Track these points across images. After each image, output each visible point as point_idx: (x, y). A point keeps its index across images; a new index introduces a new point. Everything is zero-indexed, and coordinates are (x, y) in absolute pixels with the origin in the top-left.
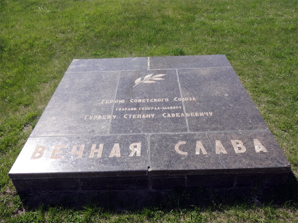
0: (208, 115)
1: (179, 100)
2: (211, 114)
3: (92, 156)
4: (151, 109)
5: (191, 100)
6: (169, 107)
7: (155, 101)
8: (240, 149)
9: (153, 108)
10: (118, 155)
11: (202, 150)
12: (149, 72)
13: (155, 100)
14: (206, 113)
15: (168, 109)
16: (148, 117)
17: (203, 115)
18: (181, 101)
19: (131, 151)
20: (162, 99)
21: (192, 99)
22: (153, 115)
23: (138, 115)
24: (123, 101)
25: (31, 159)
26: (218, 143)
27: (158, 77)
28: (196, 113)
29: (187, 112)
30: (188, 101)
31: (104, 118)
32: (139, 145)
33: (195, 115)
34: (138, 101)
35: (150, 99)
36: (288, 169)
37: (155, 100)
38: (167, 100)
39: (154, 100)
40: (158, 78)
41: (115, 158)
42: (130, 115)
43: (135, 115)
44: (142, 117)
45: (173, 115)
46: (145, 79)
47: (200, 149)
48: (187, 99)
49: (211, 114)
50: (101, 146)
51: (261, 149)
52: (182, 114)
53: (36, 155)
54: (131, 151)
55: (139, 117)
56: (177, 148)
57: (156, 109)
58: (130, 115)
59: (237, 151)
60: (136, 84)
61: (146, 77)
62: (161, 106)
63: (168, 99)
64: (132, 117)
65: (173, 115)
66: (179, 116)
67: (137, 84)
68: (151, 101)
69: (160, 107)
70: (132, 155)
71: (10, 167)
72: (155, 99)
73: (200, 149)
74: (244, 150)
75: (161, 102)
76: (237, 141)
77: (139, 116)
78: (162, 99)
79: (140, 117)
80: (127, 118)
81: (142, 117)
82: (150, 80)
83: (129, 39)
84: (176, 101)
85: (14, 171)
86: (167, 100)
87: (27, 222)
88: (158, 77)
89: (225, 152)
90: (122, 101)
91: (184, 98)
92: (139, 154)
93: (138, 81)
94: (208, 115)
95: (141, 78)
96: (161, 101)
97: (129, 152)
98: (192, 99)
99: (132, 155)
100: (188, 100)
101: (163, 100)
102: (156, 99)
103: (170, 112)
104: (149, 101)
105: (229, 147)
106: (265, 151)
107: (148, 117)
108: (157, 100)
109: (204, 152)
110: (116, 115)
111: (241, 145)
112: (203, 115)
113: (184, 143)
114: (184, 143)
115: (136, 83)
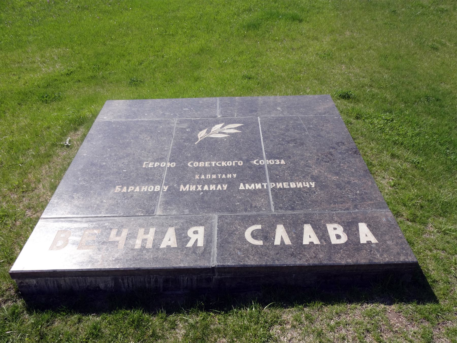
0: (308, 186)
1: (262, 164)
5: (279, 163)
6: (226, 175)
7: (223, 165)
8: (338, 237)
12: (217, 123)
13: (207, 164)
14: (306, 184)
17: (302, 187)
18: (264, 165)
19: (190, 238)
20: (234, 162)
21: (280, 162)
24: (173, 165)
25: (51, 248)
27: (231, 129)
28: (291, 183)
29: (272, 180)
30: (275, 164)
32: (201, 230)
33: (290, 187)
34: (199, 165)
37: (207, 164)
39: (220, 164)
43: (286, 183)
45: (213, 187)
46: (212, 131)
48: (272, 162)
49: (235, 176)
51: (311, 240)
53: (188, 244)
54: (190, 238)
57: (203, 177)
59: (334, 241)
60: (199, 140)
61: (213, 128)
62: (217, 174)
63: (242, 162)
65: (213, 187)
67: (201, 139)
68: (217, 164)
70: (190, 244)
71: (11, 261)
73: (282, 237)
74: (344, 239)
75: (204, 168)
76: (336, 225)
77: (208, 176)
78: (234, 162)
79: (209, 178)
82: (219, 133)
84: (256, 164)
87: (13, 341)
88: (231, 129)
92: (201, 244)
93: (202, 134)
97: (188, 239)
98: (280, 162)
99: (190, 244)
100: (273, 163)
101: (236, 163)
103: (209, 182)
104: (215, 164)
108: (226, 163)
109: (288, 242)
111: (340, 230)
112: (302, 187)
113: (259, 227)
114: (259, 227)
115: (199, 137)
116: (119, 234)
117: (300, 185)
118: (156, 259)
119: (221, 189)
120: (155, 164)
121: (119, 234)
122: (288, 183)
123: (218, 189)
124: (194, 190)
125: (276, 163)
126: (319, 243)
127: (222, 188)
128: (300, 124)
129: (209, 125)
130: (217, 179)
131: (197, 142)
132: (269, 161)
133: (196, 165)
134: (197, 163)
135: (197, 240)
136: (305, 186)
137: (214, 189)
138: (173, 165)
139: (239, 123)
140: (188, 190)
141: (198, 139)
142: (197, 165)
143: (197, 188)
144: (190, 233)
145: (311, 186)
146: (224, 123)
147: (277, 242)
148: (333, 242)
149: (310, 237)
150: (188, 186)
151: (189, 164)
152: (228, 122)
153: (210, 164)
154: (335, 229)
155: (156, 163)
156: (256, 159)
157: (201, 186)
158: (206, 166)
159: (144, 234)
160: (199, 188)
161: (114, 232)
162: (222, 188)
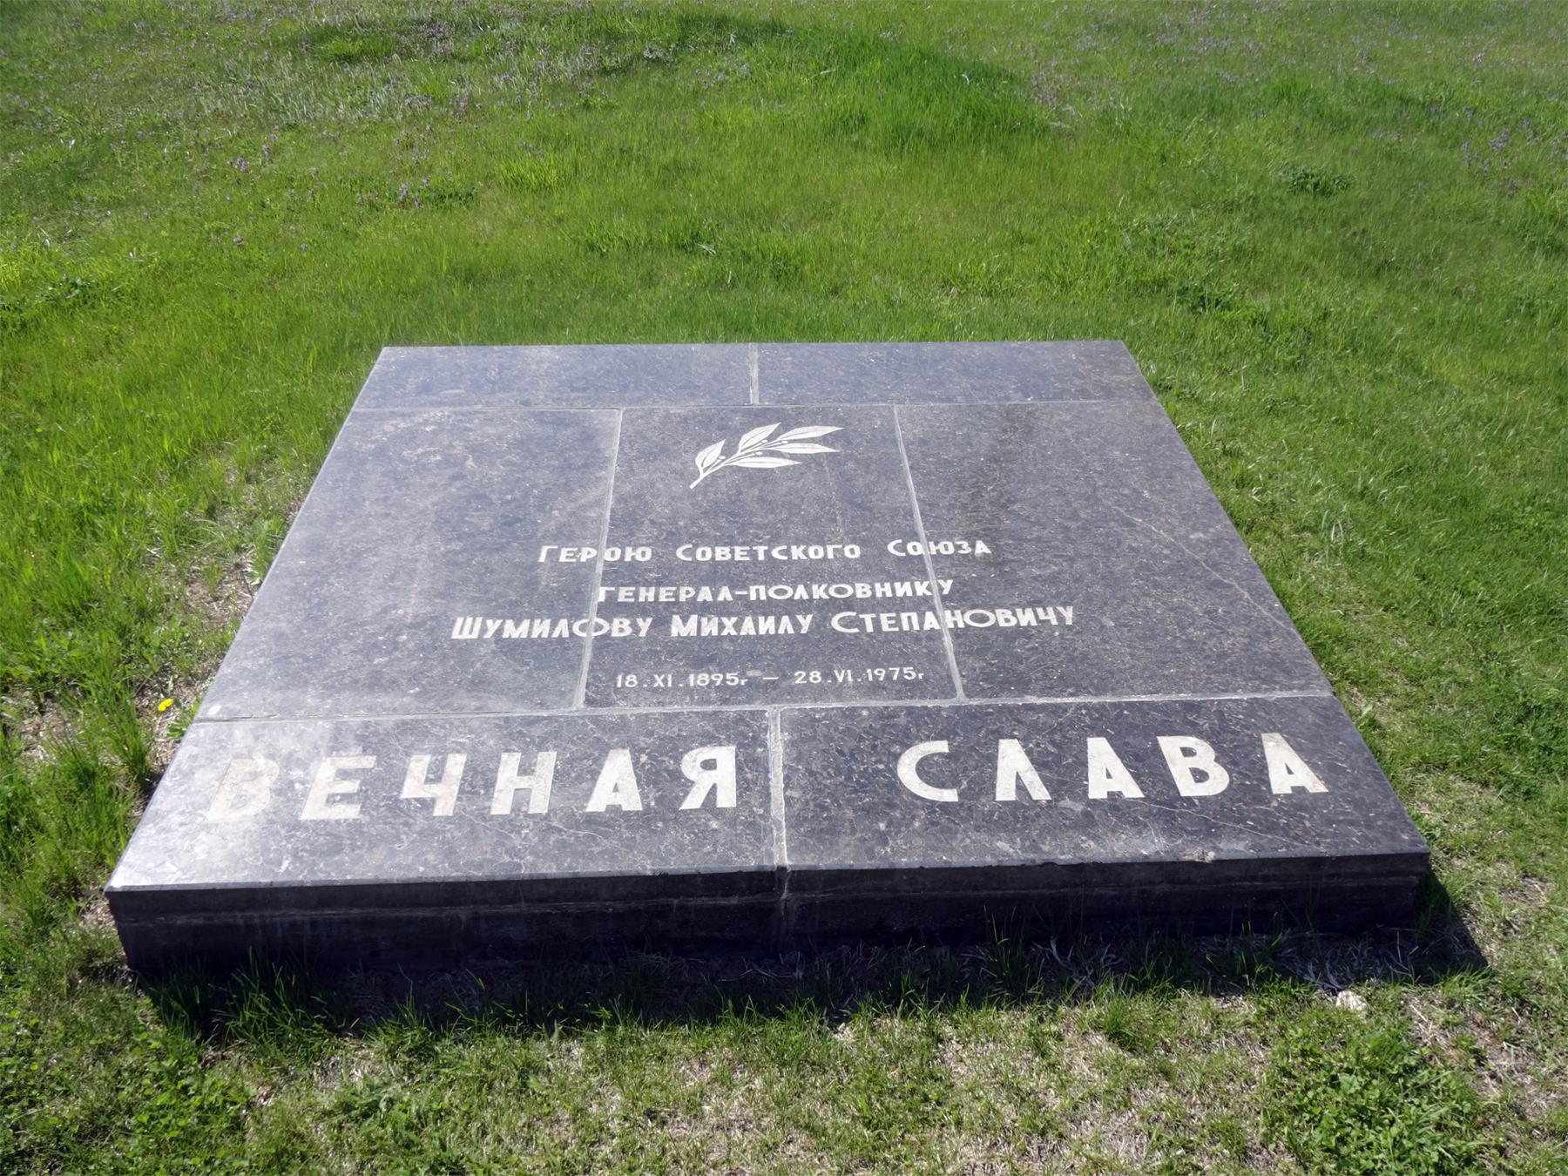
0: (1054, 622)
2: (1069, 614)
3: (501, 805)
4: (676, 595)
5: (968, 551)
6: (808, 589)
7: (795, 558)
8: (1200, 776)
9: (693, 593)
10: (631, 801)
11: (1026, 781)
12: (758, 417)
15: (720, 598)
16: (884, 593)
17: (1034, 623)
18: (921, 556)
20: (830, 549)
22: (806, 622)
23: (904, 616)
24: (643, 554)
26: (1100, 751)
27: (806, 441)
31: (331, 800)
32: (725, 756)
33: (901, 628)
35: (771, 548)
36: (1423, 858)
38: (852, 551)
40: (806, 445)
41: (614, 810)
42: (868, 618)
44: (921, 623)
46: (741, 446)
47: (1018, 777)
48: (946, 548)
49: (1069, 614)
50: (548, 761)
52: (929, 616)
55: (911, 625)
56: (907, 772)
58: (868, 618)
59: (1187, 787)
60: (702, 476)
61: (745, 437)
64: (876, 622)
66: (897, 629)
67: (709, 472)
68: (775, 553)
69: (732, 588)
70: (693, 801)
72: (794, 548)
73: (1018, 777)
74: (1218, 781)
76: (1190, 741)
77: (471, 632)
79: (916, 627)
80: (950, 796)
81: (921, 623)
83: (58, 329)
85: (122, 878)
86: (852, 551)
88: (806, 441)
89: (1132, 791)
90: (640, 550)
91: (936, 544)
92: (727, 799)
93: (709, 458)
94: (1054, 622)
95: (722, 443)
96: (826, 553)
98: (973, 546)
99: (693, 801)
101: (550, 553)
102: (802, 548)
104: (767, 553)
105: (1145, 765)
106: (1316, 786)
107: (884, 593)
109: (1040, 793)
110: (810, 617)
111: (1205, 755)
112: (1034, 623)
113: (942, 747)
114: (942, 747)
116: (436, 775)
117: (1027, 618)
118: (480, 866)
119: (791, 631)
120: (579, 551)
121: (436, 775)
122: (894, 615)
123: (556, 635)
124: (715, 633)
125: (961, 552)
126: (1139, 794)
127: (796, 625)
128: (668, 416)
129: (728, 431)
130: (692, 602)
131: (695, 483)
132: (936, 544)
133: (704, 554)
134: (708, 550)
135: (714, 787)
136: (1042, 616)
137: (772, 632)
138: (643, 554)
139: (825, 423)
140: (545, 635)
141: (696, 475)
142: (821, 555)
143: (721, 626)
144: (690, 765)
145: (1061, 618)
146: (776, 426)
147: (1005, 791)
148: (1184, 793)
149: (616, 789)
150: (526, 623)
151: (891, 547)
152: (788, 422)
153: (754, 554)
154: (1188, 752)
155: (683, 590)
156: (686, 543)
157: (734, 619)
158: (737, 558)
159: (428, 781)
160: (729, 630)
161: (419, 765)
162: (796, 625)
